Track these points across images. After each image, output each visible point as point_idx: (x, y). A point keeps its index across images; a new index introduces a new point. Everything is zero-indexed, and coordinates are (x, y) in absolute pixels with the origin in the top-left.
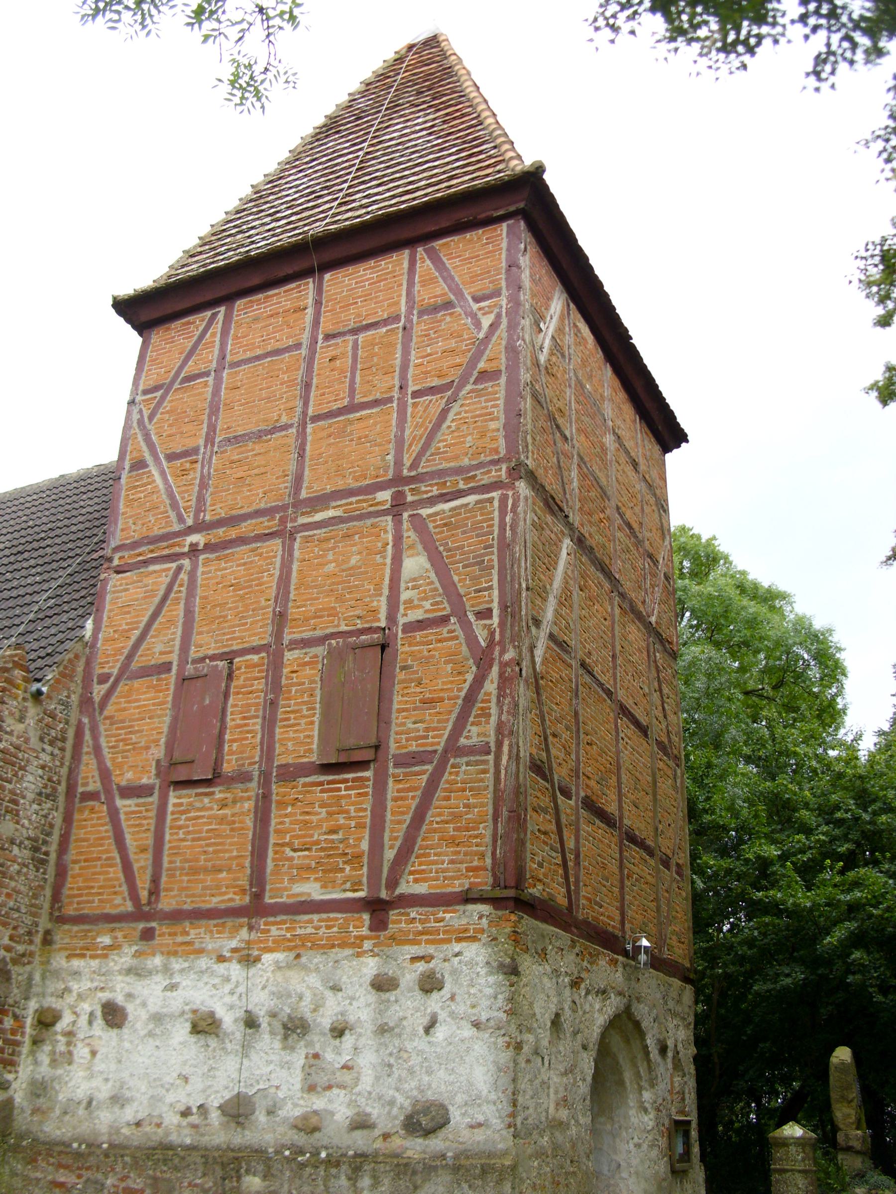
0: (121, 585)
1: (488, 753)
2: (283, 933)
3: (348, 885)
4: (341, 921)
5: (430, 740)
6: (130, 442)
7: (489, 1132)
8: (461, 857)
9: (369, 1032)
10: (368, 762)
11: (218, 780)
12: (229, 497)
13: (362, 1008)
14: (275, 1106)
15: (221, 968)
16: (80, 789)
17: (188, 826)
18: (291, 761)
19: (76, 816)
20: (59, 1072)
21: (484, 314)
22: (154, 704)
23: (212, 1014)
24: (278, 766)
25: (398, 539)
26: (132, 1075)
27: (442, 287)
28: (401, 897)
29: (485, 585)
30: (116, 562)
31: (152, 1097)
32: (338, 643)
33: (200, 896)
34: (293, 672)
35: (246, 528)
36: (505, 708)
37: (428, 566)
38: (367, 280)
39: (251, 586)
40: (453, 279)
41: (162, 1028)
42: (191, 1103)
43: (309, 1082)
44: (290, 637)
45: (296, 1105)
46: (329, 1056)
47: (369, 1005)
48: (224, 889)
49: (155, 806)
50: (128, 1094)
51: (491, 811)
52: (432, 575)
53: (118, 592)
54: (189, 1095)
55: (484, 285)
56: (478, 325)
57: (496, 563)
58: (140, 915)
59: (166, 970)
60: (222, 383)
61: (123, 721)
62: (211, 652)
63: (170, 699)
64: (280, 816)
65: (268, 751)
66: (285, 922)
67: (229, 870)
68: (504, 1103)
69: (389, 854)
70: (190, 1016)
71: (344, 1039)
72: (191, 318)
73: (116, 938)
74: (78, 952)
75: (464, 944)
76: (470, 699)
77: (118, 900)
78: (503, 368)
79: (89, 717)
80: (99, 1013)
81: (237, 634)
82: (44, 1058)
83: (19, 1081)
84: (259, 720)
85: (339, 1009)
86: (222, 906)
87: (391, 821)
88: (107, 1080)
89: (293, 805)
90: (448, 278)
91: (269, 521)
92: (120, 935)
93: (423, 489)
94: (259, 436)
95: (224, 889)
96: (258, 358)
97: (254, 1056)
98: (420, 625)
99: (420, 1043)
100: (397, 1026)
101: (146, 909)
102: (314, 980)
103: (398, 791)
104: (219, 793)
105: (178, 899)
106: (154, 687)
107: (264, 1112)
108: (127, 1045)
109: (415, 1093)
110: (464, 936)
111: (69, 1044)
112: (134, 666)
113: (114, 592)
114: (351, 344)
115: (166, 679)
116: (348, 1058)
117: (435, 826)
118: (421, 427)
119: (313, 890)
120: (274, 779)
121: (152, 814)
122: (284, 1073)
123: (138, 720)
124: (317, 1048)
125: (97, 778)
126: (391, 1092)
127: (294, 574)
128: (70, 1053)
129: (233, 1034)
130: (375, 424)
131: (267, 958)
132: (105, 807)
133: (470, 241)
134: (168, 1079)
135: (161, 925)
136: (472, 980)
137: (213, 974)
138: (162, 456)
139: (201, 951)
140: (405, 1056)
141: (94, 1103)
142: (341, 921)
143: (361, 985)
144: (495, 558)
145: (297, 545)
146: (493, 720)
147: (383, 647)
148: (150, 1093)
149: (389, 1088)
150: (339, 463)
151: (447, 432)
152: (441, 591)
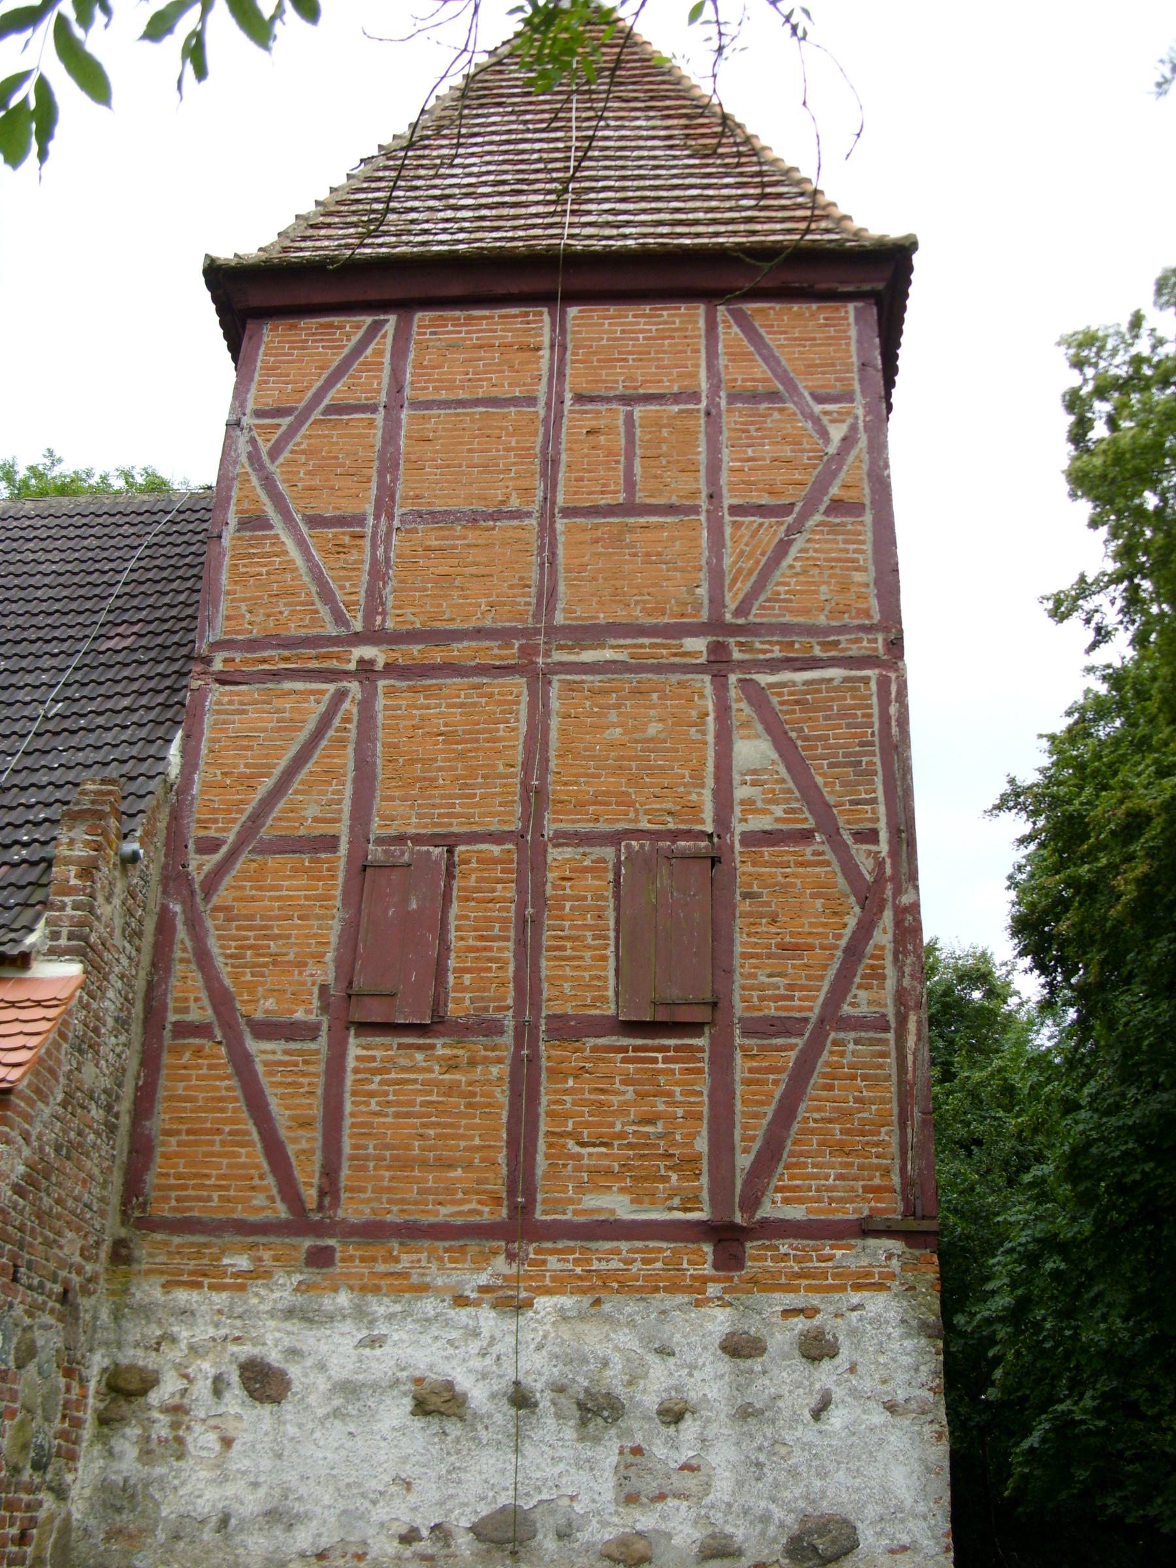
0: (231, 703)
1: (886, 1029)
2: (570, 1266)
3: (676, 1201)
4: (668, 1253)
5: (797, 1003)
6: (236, 485)
7: (918, 1559)
8: (854, 1171)
9: (722, 1416)
10: (701, 1025)
11: (439, 1027)
12: (428, 601)
13: (711, 1382)
14: (570, 1525)
15: (463, 1315)
16: (172, 1017)
17: (386, 1094)
18: (570, 1012)
19: (166, 1059)
20: (159, 1470)
21: (832, 421)
22: (307, 898)
23: (449, 1385)
24: (548, 1017)
25: (723, 710)
26: (303, 1478)
27: (761, 369)
28: (765, 1222)
29: (864, 796)
30: (218, 665)
31: (345, 1512)
32: (642, 846)
33: (416, 1203)
34: (563, 879)
35: (458, 651)
36: (907, 970)
37: (775, 756)
38: (642, 331)
39: (477, 741)
40: (778, 362)
41: (358, 1405)
42: (418, 1522)
43: (626, 1490)
44: (555, 826)
45: (605, 1524)
46: (659, 1450)
47: (722, 1377)
48: (460, 1195)
49: (323, 1057)
50: (298, 1507)
51: (895, 1111)
52: (782, 769)
53: (226, 712)
54: (414, 1509)
55: (828, 381)
56: (824, 435)
57: (879, 768)
58: (300, 1222)
59: (360, 1314)
60: (399, 427)
61: (252, 917)
62: (412, 831)
63: (338, 892)
64: (556, 1091)
65: (528, 987)
66: (572, 1251)
67: (469, 1166)
68: (939, 1517)
69: (744, 1161)
70: (410, 1386)
71: (683, 1426)
72: (336, 320)
73: (260, 1259)
74: (185, 1278)
75: (866, 1294)
76: (854, 952)
77: (259, 1200)
78: (867, 502)
79: (183, 903)
80: (234, 1378)
81: (458, 810)
82: (127, 1445)
83: (78, 1485)
84: (511, 945)
85: (671, 1382)
86: (459, 1221)
87: (743, 1112)
88: (255, 1485)
89: (576, 1077)
90: (770, 359)
91: (500, 647)
92: (267, 1255)
93: (758, 646)
94: (474, 519)
95: (460, 1195)
96: (461, 403)
97: (528, 1449)
98: (768, 837)
99: (807, 1432)
100: (769, 1408)
101: (317, 1217)
102: (626, 1339)
103: (751, 1071)
104: (442, 1047)
105: (375, 1205)
106: (306, 870)
107: (552, 1535)
108: (292, 1430)
109: (801, 1504)
110: (864, 1282)
111: (175, 1426)
112: (265, 833)
113: (218, 712)
114: (622, 417)
115: (327, 861)
116: (691, 1453)
117: (812, 1124)
118: (749, 557)
119: (617, 1204)
120: (542, 1036)
121: (320, 1068)
122: (584, 1476)
123: (278, 918)
124: (639, 1439)
125: (206, 1002)
126: (763, 1504)
127: (554, 735)
128: (180, 1441)
129: (490, 1416)
130: (672, 539)
131: (543, 1303)
132: (223, 1050)
133: (800, 315)
134: (373, 1484)
135: (345, 1244)
136: (881, 1344)
137: (447, 1323)
138: (298, 518)
139: (423, 1289)
140: (783, 1450)
141: (233, 1522)
142: (668, 1253)
143: (705, 1348)
144: (877, 760)
145: (553, 692)
146: (890, 983)
147: (715, 861)
148: (341, 1506)
149: (760, 1496)
150: (618, 583)
151: (789, 572)
152: (797, 794)
